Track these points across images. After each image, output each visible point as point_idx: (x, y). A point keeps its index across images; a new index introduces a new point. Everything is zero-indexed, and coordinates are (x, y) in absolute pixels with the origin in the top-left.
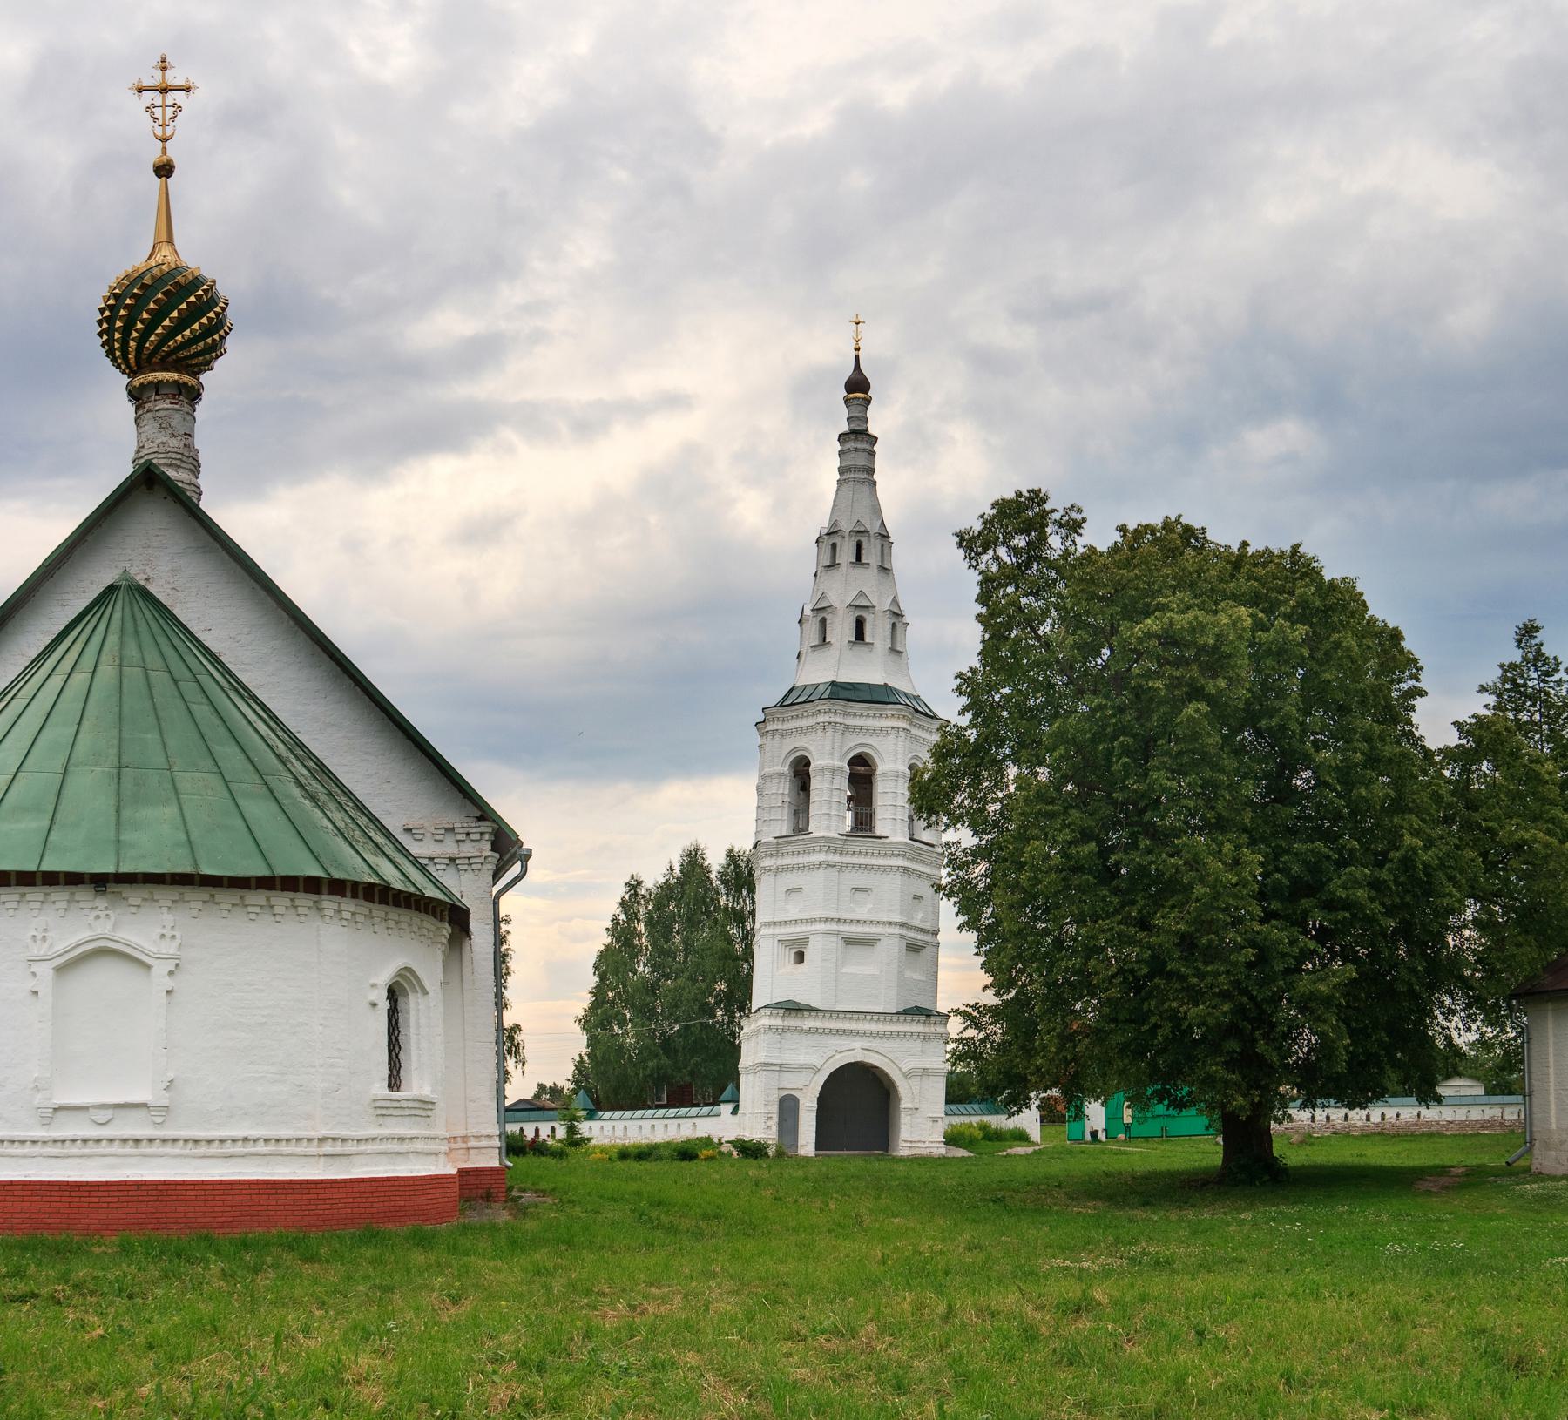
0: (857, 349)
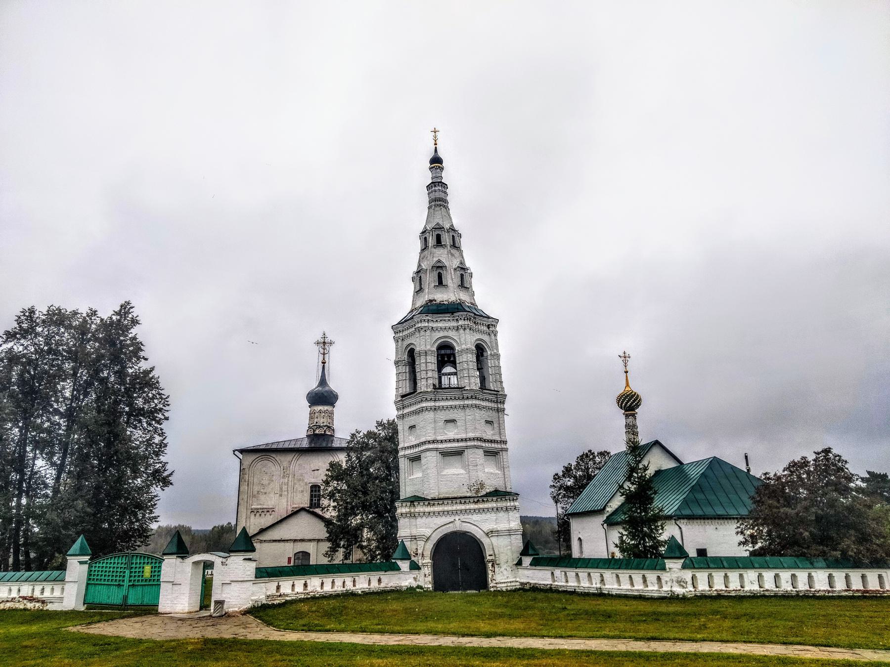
0: (436, 144)
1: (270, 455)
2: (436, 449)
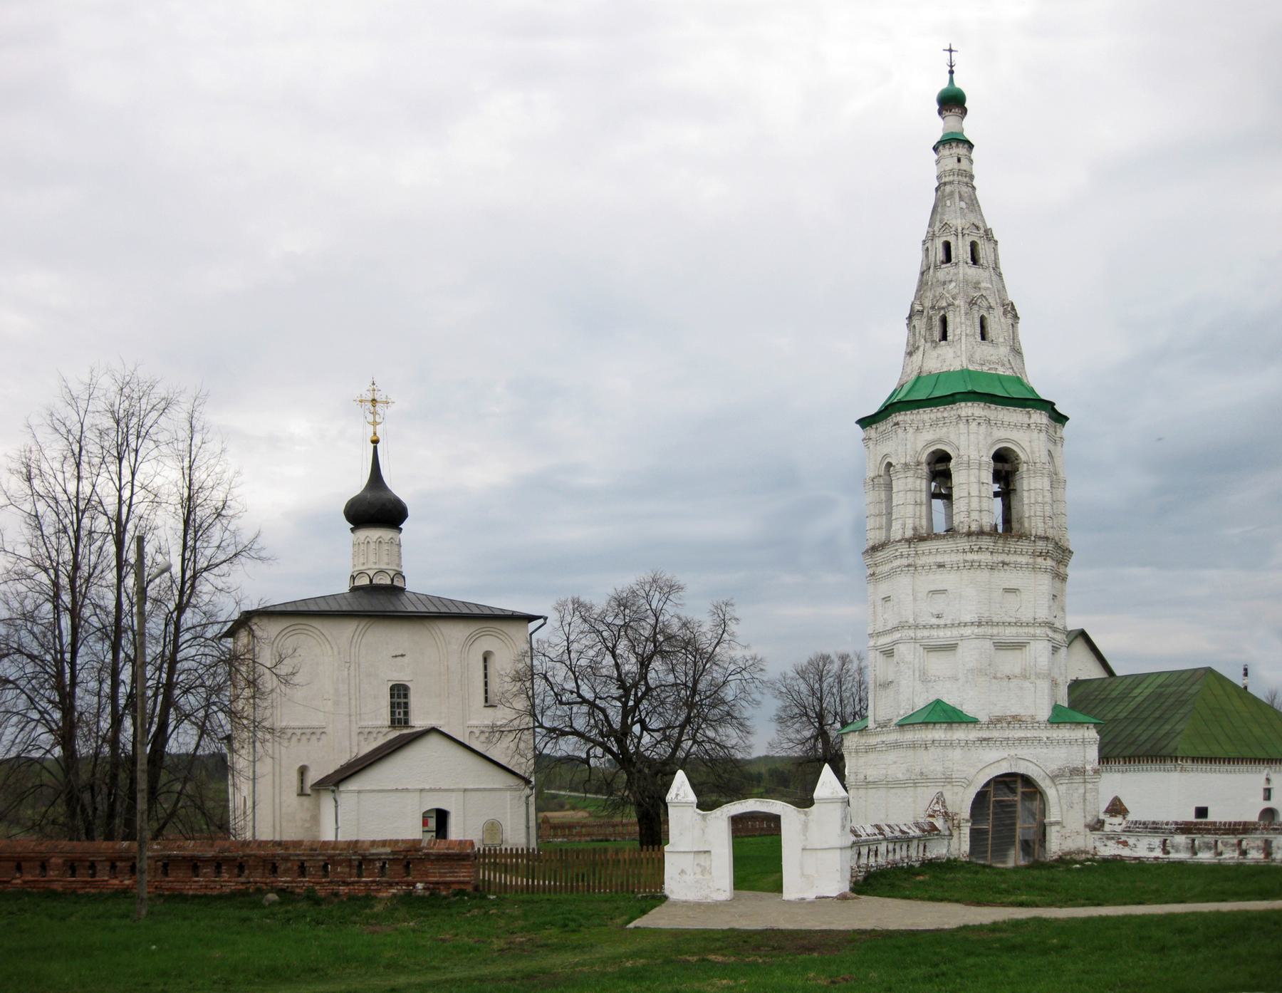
1: (313, 625)
2: (915, 640)
